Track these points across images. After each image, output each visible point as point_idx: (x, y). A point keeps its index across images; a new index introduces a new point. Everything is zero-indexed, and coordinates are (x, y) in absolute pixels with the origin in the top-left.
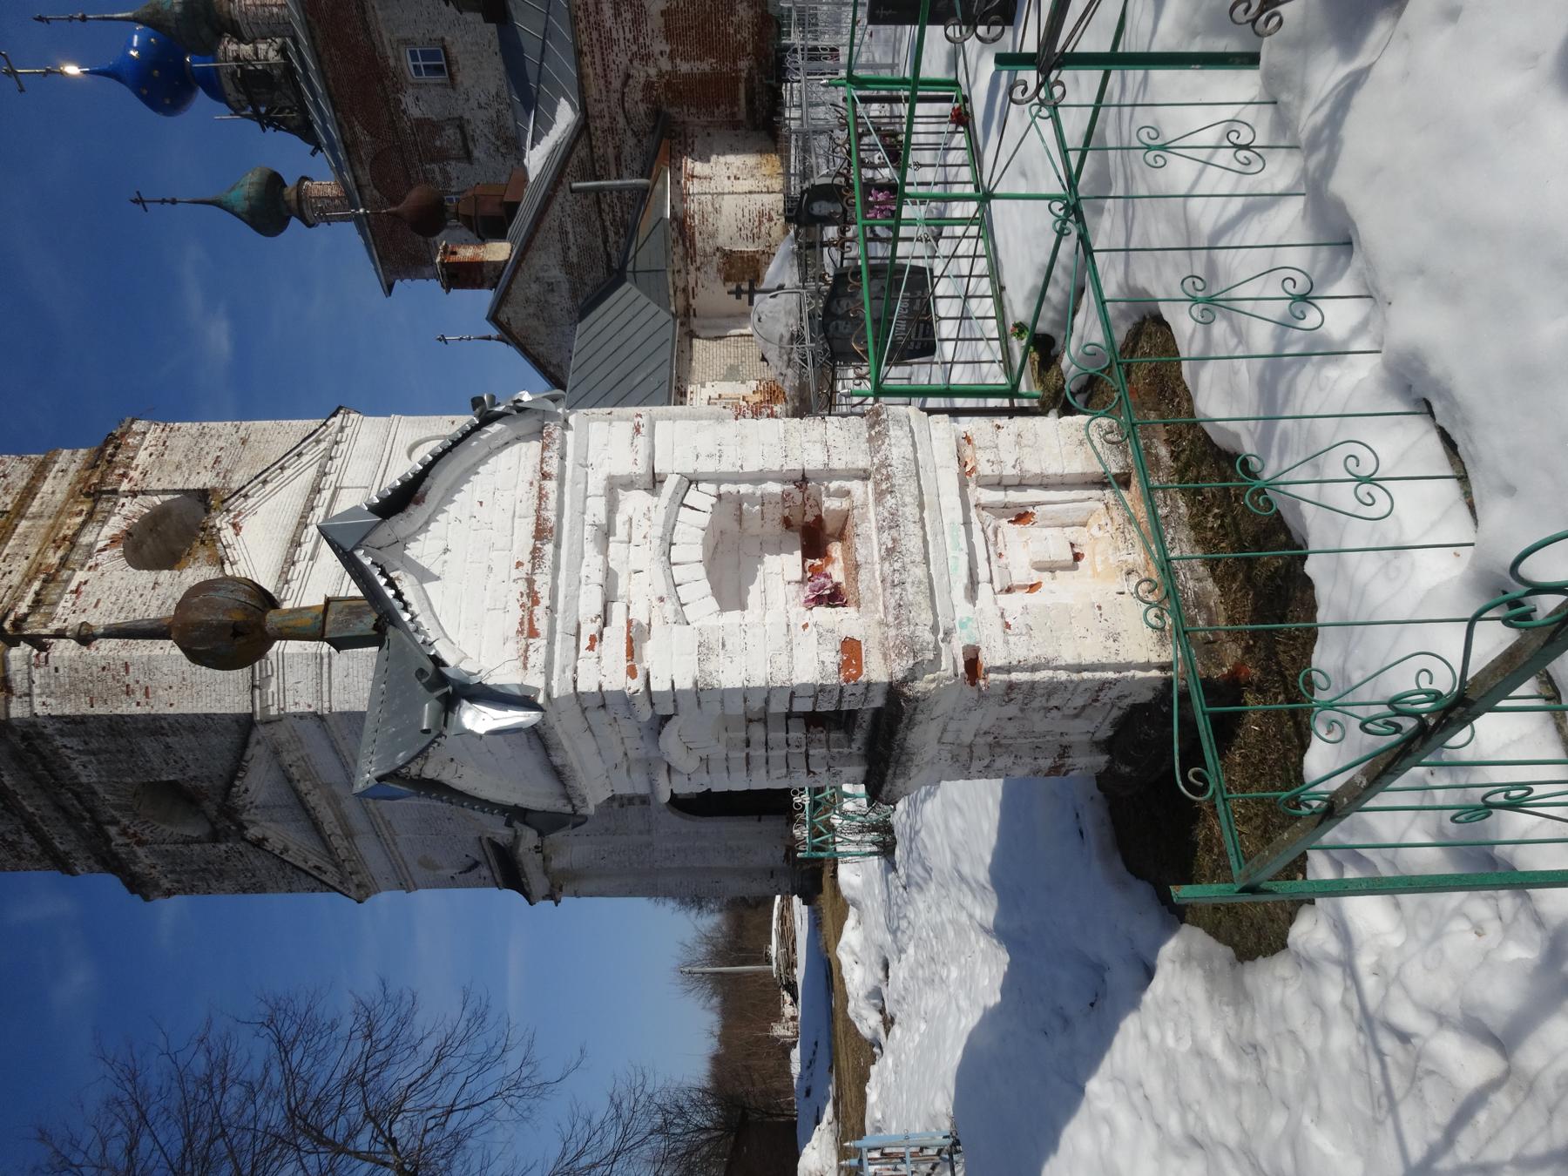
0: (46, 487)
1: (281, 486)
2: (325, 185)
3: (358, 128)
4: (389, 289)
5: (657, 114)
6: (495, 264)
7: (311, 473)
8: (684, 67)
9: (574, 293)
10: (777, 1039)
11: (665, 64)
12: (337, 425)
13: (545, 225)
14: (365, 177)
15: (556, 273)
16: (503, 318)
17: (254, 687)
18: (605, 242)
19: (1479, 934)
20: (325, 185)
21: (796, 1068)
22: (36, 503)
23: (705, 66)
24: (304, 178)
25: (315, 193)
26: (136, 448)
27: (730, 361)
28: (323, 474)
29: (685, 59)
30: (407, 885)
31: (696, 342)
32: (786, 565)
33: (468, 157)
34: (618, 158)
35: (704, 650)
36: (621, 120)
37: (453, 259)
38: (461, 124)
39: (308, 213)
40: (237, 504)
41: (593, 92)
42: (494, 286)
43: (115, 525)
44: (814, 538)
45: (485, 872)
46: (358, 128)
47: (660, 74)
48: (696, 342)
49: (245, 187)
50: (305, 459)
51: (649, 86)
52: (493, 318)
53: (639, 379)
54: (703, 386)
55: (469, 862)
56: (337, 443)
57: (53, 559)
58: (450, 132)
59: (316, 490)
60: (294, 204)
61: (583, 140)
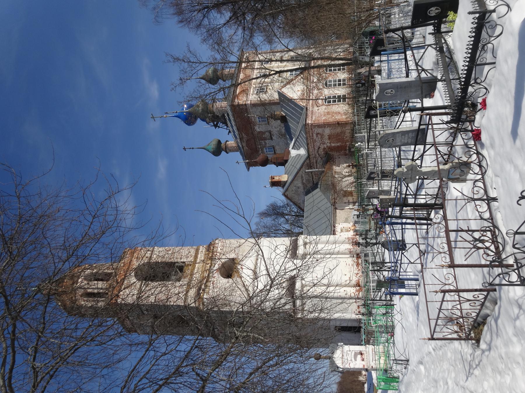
0: (199, 256)
2: (232, 143)
3: (243, 134)
4: (248, 169)
5: (326, 153)
6: (284, 182)
8: (333, 145)
9: (304, 189)
10: (360, 381)
11: (329, 145)
13: (298, 175)
14: (244, 144)
15: (300, 185)
16: (286, 194)
18: (313, 178)
20: (232, 143)
22: (198, 260)
23: (339, 144)
24: (227, 141)
25: (230, 146)
26: (217, 248)
27: (346, 217)
29: (333, 143)
31: (337, 210)
32: (359, 356)
33: (272, 139)
34: (316, 162)
36: (318, 155)
37: (274, 180)
38: (270, 132)
39: (228, 151)
40: (241, 263)
41: (311, 150)
42: (283, 187)
43: (217, 267)
44: (362, 354)
46: (243, 134)
47: (327, 146)
48: (337, 210)
49: (212, 146)
51: (324, 149)
52: (284, 194)
53: (324, 221)
57: (206, 274)
58: (267, 134)
60: (224, 149)
61: (308, 159)
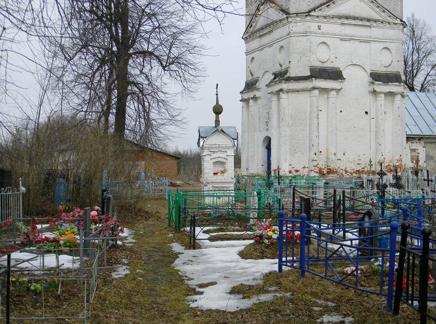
1: (371, 8)
7: (377, 17)
12: (397, 22)
17: (297, 14)
19: (214, 173)
21: (383, 228)
28: (375, 21)
30: (247, 53)
35: (208, 161)
45: (250, 78)
50: (383, 14)
54: (423, 147)
55: (253, 73)
56: (389, 23)
59: (369, 20)
